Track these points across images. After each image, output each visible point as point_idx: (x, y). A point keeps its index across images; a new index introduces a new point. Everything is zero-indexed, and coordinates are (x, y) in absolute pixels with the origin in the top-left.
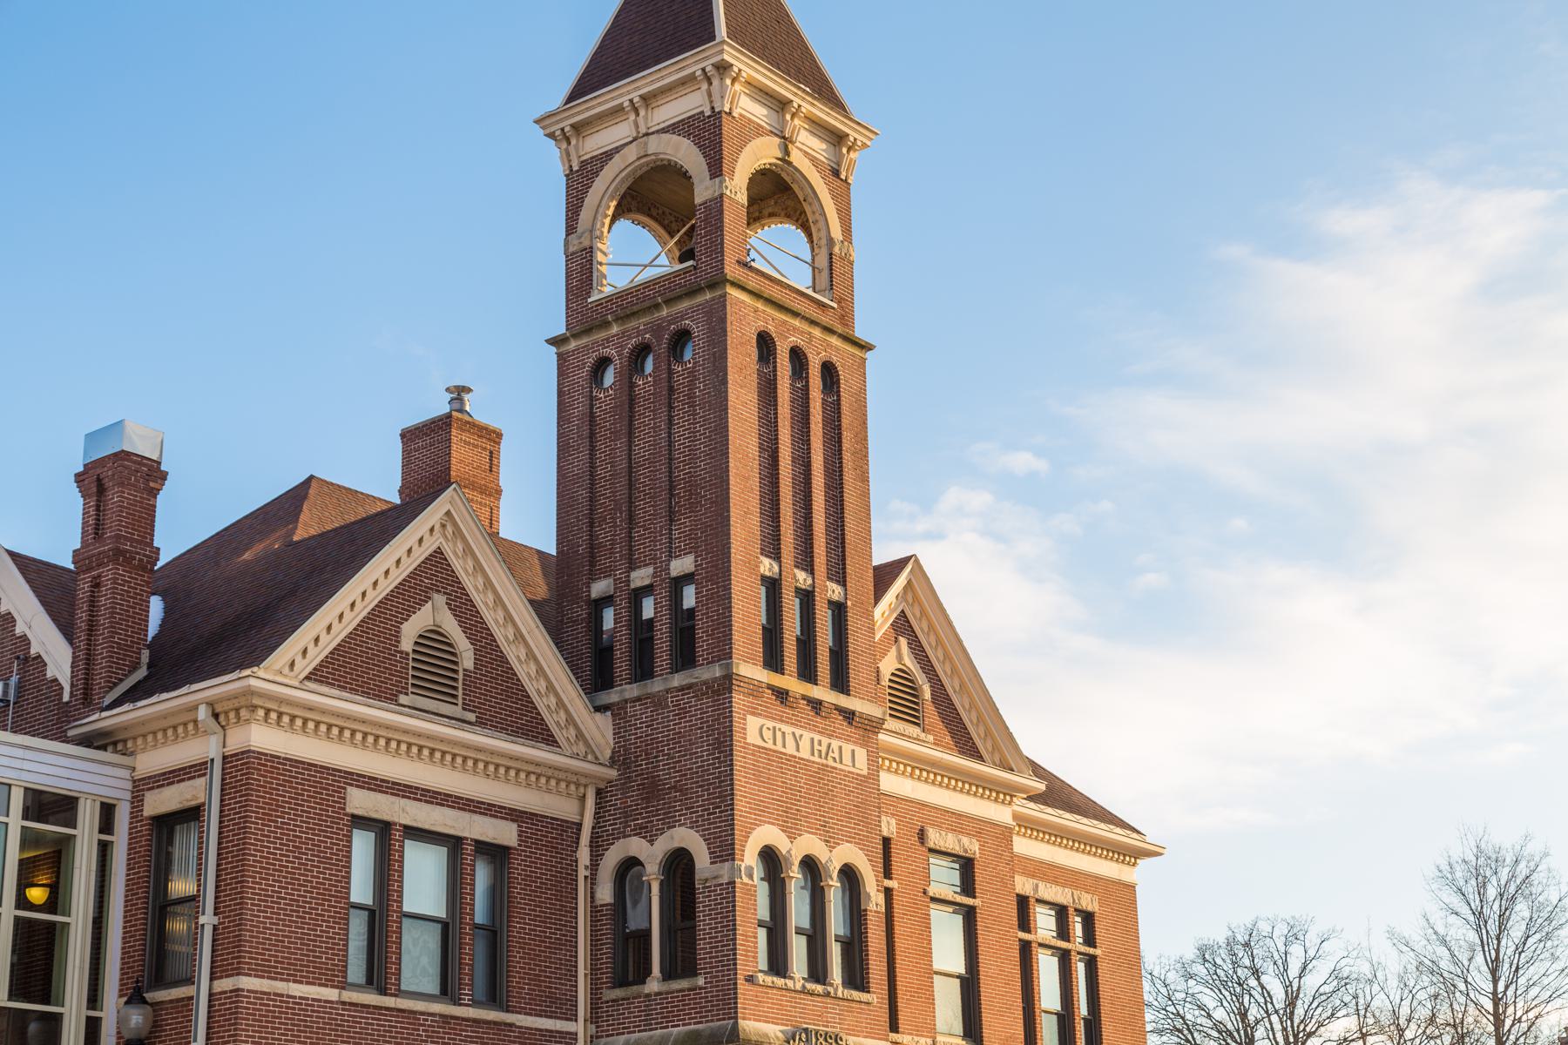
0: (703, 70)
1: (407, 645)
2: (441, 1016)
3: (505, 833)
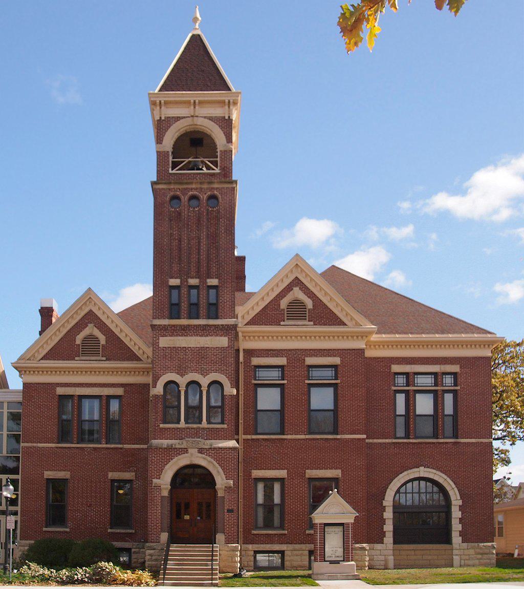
0: (160, 101)
1: (78, 342)
2: (93, 448)
3: (120, 391)
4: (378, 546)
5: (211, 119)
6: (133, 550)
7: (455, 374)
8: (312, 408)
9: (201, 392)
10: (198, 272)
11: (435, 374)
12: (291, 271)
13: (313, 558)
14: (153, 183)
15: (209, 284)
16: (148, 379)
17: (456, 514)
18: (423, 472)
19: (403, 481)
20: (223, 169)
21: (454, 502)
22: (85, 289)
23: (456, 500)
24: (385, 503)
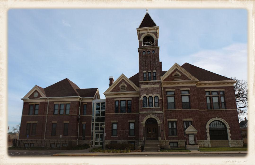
4: (206, 141)
5: (152, 33)
6: (135, 142)
7: (223, 91)
8: (183, 102)
9: (153, 99)
10: (150, 69)
11: (218, 91)
12: (175, 67)
13: (186, 144)
14: (138, 49)
15: (153, 72)
16: (138, 96)
17: (229, 131)
18: (217, 119)
19: (211, 121)
20: (156, 44)
21: (227, 128)
22: (122, 74)
23: (228, 127)
24: (206, 128)
